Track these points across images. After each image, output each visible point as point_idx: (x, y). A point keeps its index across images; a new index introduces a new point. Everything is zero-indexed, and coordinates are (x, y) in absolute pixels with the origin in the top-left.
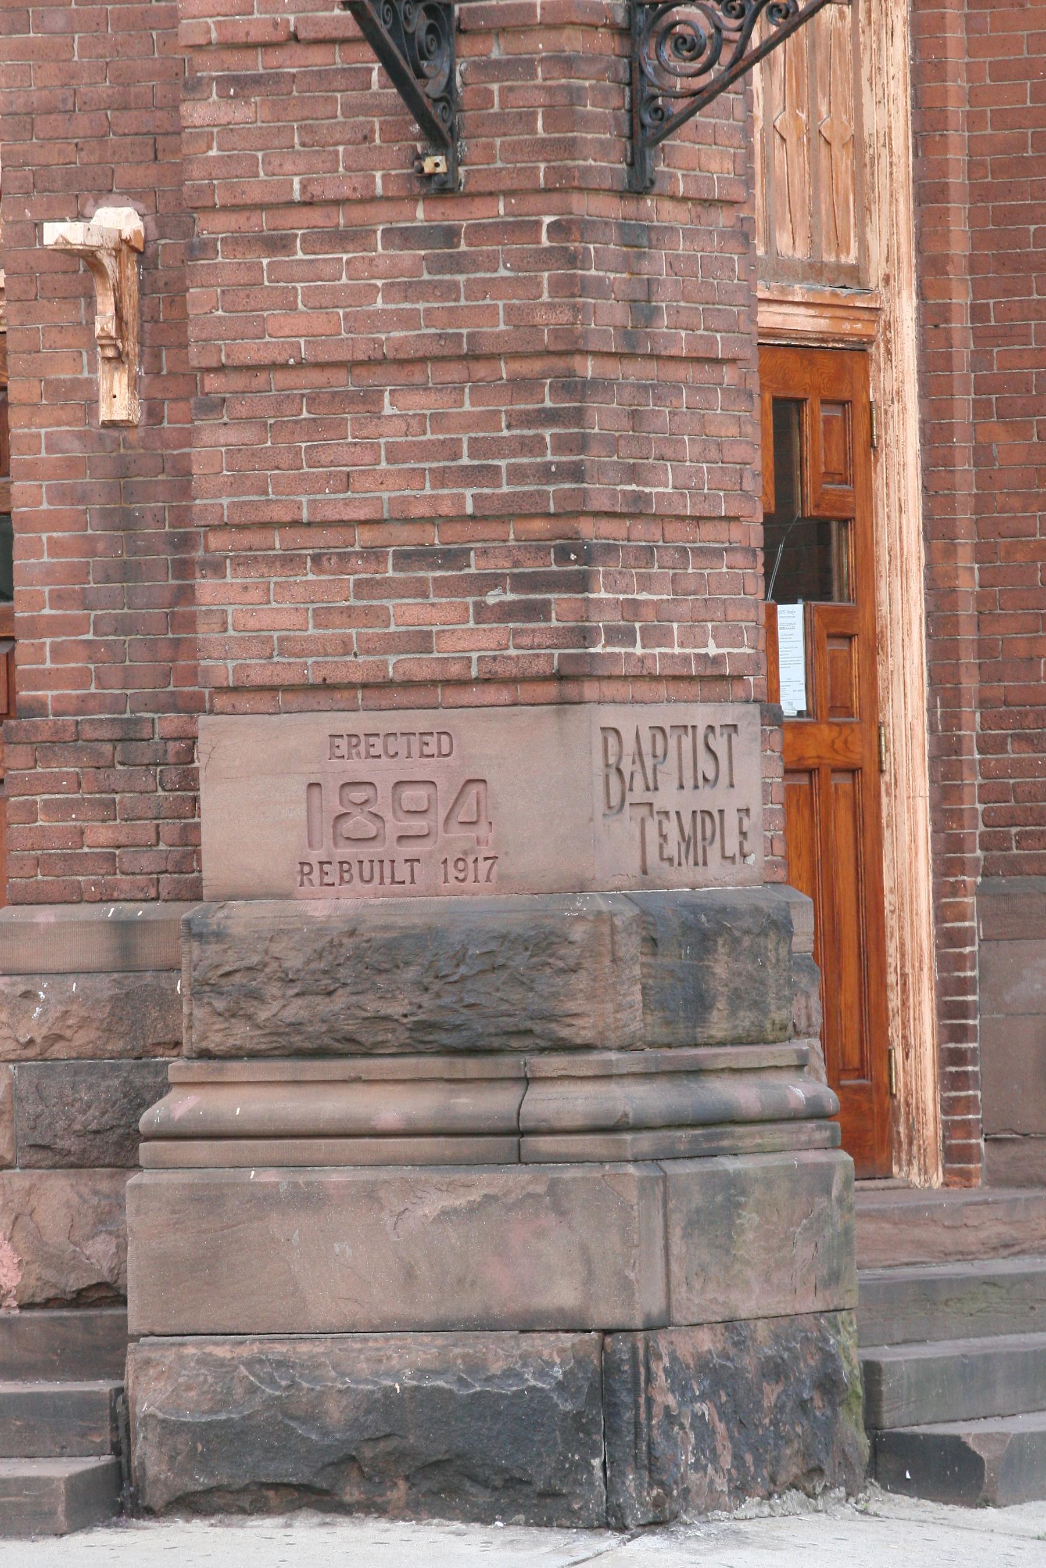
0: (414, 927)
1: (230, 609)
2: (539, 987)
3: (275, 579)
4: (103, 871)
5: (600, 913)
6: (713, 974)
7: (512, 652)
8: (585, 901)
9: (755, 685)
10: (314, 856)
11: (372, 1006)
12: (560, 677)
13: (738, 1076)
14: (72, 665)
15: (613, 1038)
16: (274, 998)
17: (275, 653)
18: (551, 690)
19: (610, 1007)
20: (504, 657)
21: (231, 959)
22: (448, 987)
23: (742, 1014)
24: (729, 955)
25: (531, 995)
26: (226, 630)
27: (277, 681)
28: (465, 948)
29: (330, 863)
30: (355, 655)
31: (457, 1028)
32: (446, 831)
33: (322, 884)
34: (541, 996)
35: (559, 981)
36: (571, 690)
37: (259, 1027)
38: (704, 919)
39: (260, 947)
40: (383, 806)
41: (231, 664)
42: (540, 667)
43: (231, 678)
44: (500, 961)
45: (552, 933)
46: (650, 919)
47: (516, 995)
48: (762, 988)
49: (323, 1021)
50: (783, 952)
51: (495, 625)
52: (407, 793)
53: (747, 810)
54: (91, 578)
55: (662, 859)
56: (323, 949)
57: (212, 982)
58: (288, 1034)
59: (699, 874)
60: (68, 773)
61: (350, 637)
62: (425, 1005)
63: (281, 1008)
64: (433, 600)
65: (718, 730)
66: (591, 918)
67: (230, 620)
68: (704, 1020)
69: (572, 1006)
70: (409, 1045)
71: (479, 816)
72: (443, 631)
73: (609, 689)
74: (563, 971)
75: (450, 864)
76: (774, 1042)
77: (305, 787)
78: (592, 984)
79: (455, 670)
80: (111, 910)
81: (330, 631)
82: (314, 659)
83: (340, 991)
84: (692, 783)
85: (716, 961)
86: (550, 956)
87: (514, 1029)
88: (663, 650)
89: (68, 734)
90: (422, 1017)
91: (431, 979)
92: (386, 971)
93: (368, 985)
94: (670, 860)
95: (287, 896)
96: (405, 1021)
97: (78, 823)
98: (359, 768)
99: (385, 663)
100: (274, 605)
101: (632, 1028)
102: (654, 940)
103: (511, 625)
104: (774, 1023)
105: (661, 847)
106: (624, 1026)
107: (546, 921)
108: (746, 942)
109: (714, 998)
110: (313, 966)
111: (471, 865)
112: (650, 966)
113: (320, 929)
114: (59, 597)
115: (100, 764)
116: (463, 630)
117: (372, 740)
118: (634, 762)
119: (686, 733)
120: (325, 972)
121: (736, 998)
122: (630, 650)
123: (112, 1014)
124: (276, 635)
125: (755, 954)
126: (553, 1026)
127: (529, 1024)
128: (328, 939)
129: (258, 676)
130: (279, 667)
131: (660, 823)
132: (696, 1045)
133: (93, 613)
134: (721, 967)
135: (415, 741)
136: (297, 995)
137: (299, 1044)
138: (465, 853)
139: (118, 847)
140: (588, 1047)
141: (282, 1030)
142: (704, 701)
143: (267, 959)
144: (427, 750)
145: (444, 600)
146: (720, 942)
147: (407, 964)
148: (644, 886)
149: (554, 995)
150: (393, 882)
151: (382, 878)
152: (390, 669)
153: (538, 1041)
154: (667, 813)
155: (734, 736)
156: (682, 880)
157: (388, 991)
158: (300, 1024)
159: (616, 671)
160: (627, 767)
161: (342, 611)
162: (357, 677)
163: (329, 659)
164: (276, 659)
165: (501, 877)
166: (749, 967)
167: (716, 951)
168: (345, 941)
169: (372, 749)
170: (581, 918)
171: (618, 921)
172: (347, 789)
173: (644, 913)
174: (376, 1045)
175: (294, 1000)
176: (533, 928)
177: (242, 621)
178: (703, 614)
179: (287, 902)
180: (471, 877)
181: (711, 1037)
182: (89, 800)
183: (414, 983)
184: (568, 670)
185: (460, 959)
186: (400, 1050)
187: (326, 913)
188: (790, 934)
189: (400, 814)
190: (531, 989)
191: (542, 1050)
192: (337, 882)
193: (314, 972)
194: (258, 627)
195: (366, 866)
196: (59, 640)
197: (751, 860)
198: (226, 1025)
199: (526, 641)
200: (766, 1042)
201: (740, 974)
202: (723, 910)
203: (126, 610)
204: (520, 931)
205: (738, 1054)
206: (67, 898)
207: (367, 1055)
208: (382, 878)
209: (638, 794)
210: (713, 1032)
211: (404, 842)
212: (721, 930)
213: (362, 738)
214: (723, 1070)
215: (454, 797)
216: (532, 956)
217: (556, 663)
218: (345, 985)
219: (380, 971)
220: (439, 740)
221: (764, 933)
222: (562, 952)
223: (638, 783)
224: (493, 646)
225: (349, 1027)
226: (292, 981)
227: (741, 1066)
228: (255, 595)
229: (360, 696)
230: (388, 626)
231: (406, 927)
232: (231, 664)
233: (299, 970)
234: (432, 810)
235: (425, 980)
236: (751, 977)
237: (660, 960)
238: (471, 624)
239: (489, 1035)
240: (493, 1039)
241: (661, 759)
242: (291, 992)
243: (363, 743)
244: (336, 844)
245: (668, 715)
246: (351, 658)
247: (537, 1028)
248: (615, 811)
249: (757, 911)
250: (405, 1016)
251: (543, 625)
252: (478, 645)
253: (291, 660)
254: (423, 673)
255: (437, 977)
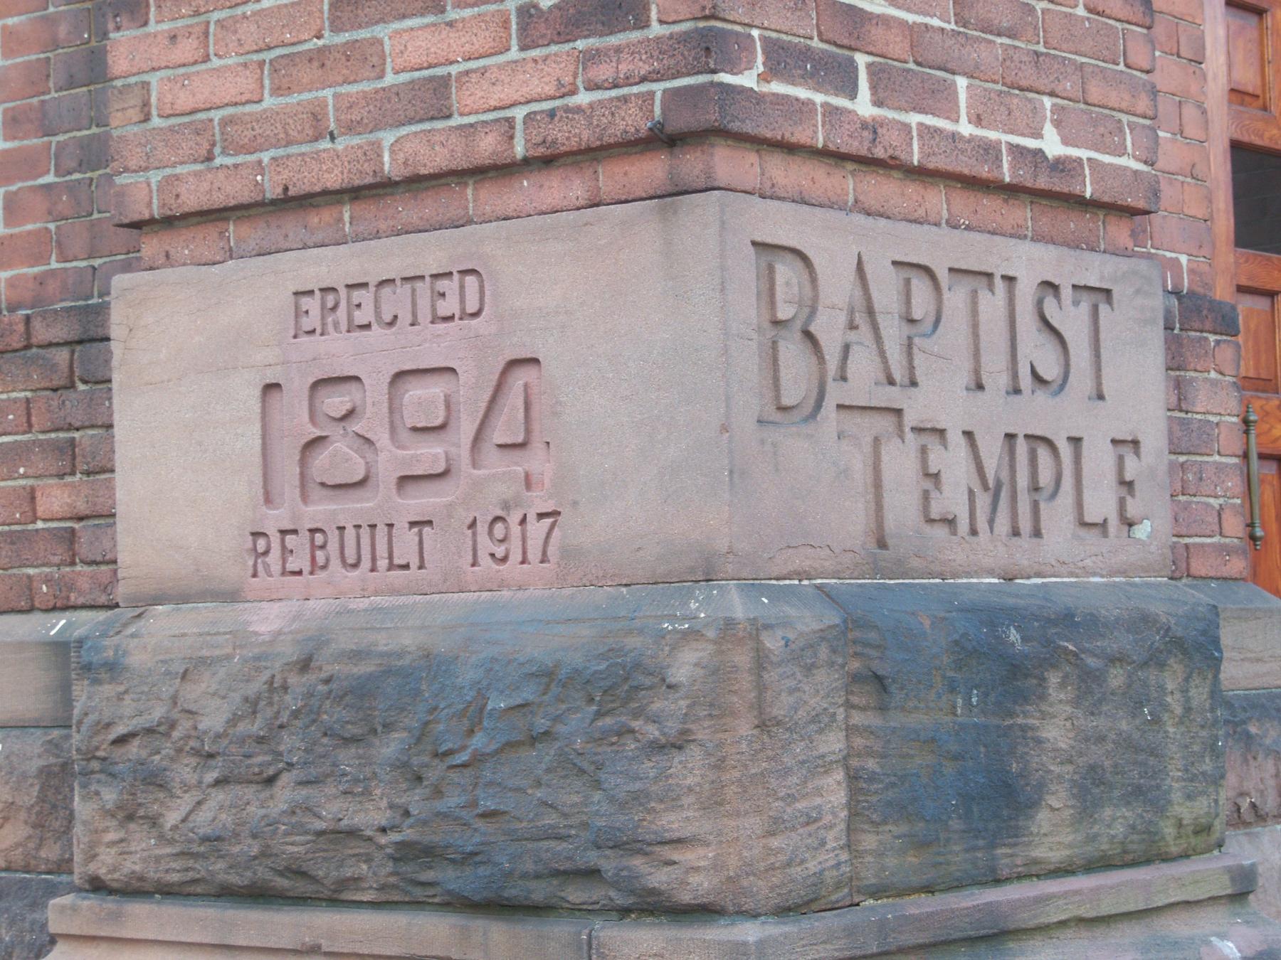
0: (400, 655)
1: (154, 79)
2: (610, 781)
3: (216, 16)
4: (56, 559)
5: (730, 623)
6: (1039, 741)
7: (583, 98)
8: (709, 598)
9: (1192, 271)
10: (274, 519)
11: (333, 808)
12: (664, 139)
13: (1099, 931)
14: (29, 227)
15: (761, 889)
16: (187, 788)
17: (217, 150)
18: (652, 170)
19: (753, 824)
20: (567, 109)
21: (128, 712)
22: (454, 776)
23: (1108, 812)
24: (1076, 702)
25: (597, 795)
26: (147, 119)
27: (218, 200)
28: (482, 696)
29: (295, 532)
30: (333, 138)
31: (469, 858)
32: (475, 465)
33: (284, 573)
34: (612, 800)
35: (648, 767)
36: (691, 164)
37: (171, 842)
38: (1014, 636)
39: (166, 690)
40: (373, 423)
41: (155, 177)
42: (633, 122)
43: (155, 206)
44: (541, 723)
45: (637, 666)
46: (872, 636)
47: (570, 797)
48: (1152, 761)
49: (254, 836)
50: (1199, 694)
51: (554, 48)
52: (415, 392)
53: (1135, 443)
54: (51, 85)
55: (931, 521)
56: (258, 699)
57: (100, 754)
58: (203, 856)
59: (1023, 553)
60: (15, 401)
61: (323, 104)
62: (414, 811)
63: (198, 807)
64: (452, 14)
65: (1066, 292)
66: (711, 634)
67: (153, 100)
68: (1016, 833)
69: (672, 822)
70: (394, 887)
71: (528, 431)
72: (467, 73)
73: (782, 171)
74: (657, 748)
75: (482, 528)
76: (1185, 856)
77: (257, 392)
78: (712, 775)
79: (487, 147)
80: (58, 624)
81: (295, 98)
82: (273, 153)
83: (285, 778)
84: (1004, 380)
85: (1044, 716)
86: (636, 715)
87: (568, 866)
88: (929, 120)
89: (16, 337)
90: (408, 834)
91: (426, 759)
92: (355, 740)
93: (326, 768)
94: (951, 522)
95: (232, 596)
96: (383, 840)
97: (30, 482)
98: (337, 351)
99: (377, 146)
100: (216, 63)
101: (812, 866)
102: (879, 679)
103: (580, 44)
104: (1180, 825)
105: (926, 496)
106: (789, 864)
107: (633, 642)
108: (1116, 678)
109: (1041, 787)
110: (242, 727)
111: (516, 530)
112: (868, 731)
113: (257, 658)
114: (14, 120)
115: (55, 383)
116: (500, 67)
117: (357, 295)
118: (852, 326)
119: (991, 288)
120: (260, 740)
121: (1091, 788)
122: (841, 102)
123: (42, 799)
124: (217, 115)
125: (1136, 700)
126: (638, 862)
127: (592, 858)
128: (265, 676)
129: (193, 197)
130: (221, 175)
131: (924, 450)
132: (998, 882)
133: (55, 139)
134: (1056, 726)
135: (423, 288)
136: (217, 783)
137: (221, 877)
138: (506, 506)
139: (80, 519)
140: (704, 911)
141: (195, 848)
142: (1038, 238)
143: (175, 714)
144: (445, 308)
145: (468, 12)
146: (1054, 679)
147: (388, 727)
148: (877, 571)
149: (639, 798)
150: (391, 567)
151: (374, 559)
152: (386, 158)
153: (612, 893)
154: (941, 432)
155: (1103, 309)
156: (981, 562)
157: (357, 781)
158: (218, 839)
159: (799, 135)
160: (830, 329)
161: (310, 57)
162: (333, 180)
163: (294, 150)
164: (218, 161)
165: (566, 553)
166: (1124, 725)
167: (1043, 697)
168: (293, 680)
169: (357, 313)
170: (693, 635)
171: (772, 643)
172: (323, 392)
173: (853, 623)
174: (344, 884)
175: (213, 791)
176: (602, 657)
177: (169, 98)
178: (1028, 76)
179: (228, 607)
180: (516, 556)
181: (1036, 862)
182: (40, 443)
183: (394, 767)
184: (680, 122)
185: (474, 716)
186: (383, 898)
187: (275, 626)
188: (1215, 663)
189: (404, 435)
190: (597, 785)
191: (624, 912)
192: (306, 568)
193: (242, 741)
194: (190, 105)
195: (350, 533)
196: (13, 188)
197: (1142, 531)
198: (122, 834)
199: (604, 72)
200: (1166, 858)
201: (1101, 739)
202: (1066, 620)
203: (94, 130)
204: (577, 659)
205: (1097, 890)
206: (13, 605)
207: (334, 902)
208: (374, 559)
209: (863, 378)
210: (1039, 853)
211: (411, 488)
212: (1052, 657)
213: (343, 292)
214: (1063, 924)
215: (487, 396)
216: (599, 715)
217: (657, 110)
218: (290, 765)
219: (348, 741)
220: (462, 287)
221: (1155, 660)
222: (656, 706)
223: (863, 365)
224: (550, 89)
225: (295, 848)
226: (211, 756)
227: (1105, 910)
228: (187, 49)
229: (347, 217)
230: (381, 76)
231: (388, 655)
232: (155, 177)
233: (218, 736)
234: (452, 424)
235: (415, 761)
236: (1127, 743)
237: (896, 719)
238: (514, 54)
239: (525, 876)
240: (533, 884)
241: (927, 326)
242: (210, 777)
243: (343, 304)
244: (305, 498)
245: (940, 248)
246: (325, 144)
247: (609, 863)
248: (796, 416)
249: (1146, 620)
250: (383, 830)
251: (635, 36)
252: (526, 91)
253: (240, 159)
254: (435, 159)
255: (436, 755)
